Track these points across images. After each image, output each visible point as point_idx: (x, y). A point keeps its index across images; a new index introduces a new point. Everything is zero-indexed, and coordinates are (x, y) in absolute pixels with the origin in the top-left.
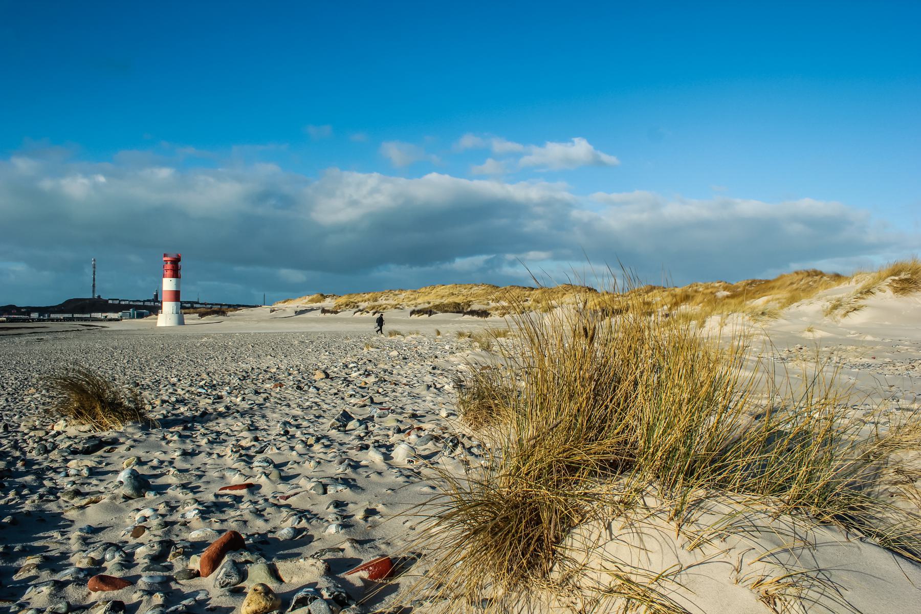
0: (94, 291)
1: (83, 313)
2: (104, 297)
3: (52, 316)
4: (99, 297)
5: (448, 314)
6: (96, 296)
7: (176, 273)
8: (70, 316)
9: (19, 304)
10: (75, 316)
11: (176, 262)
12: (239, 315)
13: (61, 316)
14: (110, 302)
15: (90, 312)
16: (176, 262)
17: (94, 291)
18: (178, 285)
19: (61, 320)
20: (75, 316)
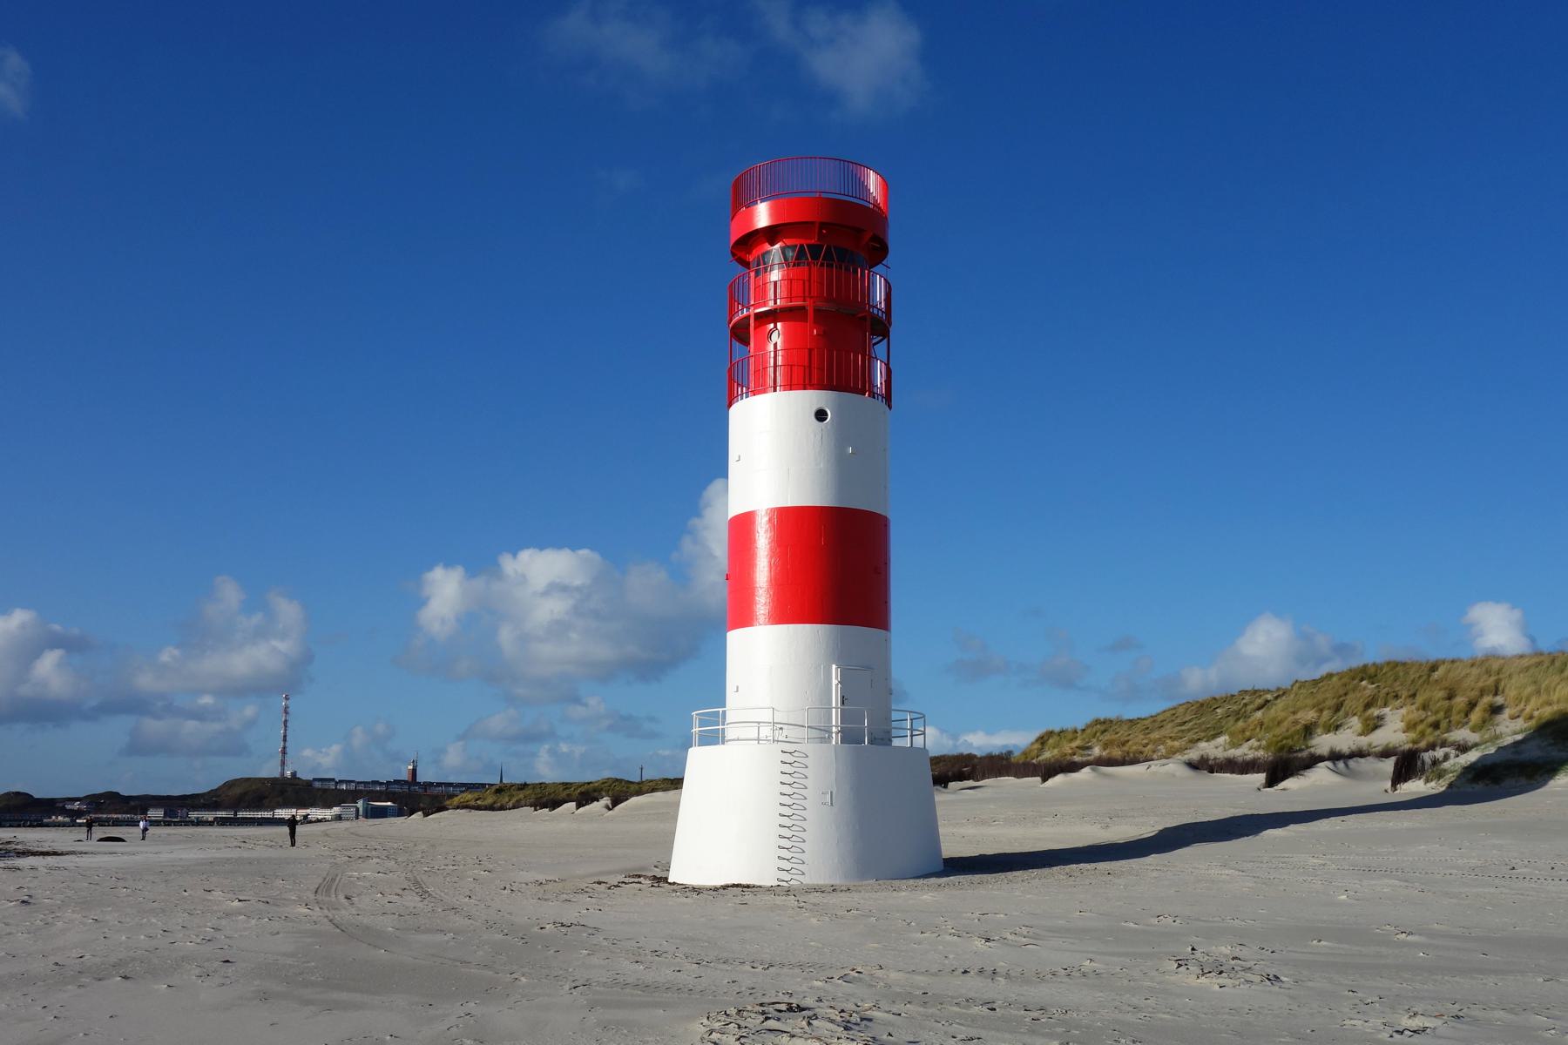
0: (283, 763)
1: (259, 808)
2: (305, 775)
3: (194, 815)
4: (294, 774)
5: (1292, 827)
6: (288, 773)
7: (840, 350)
8: (230, 814)
9: (125, 791)
10: (241, 814)
11: (842, 241)
12: (1516, 733)
13: (209, 816)
14: (317, 785)
15: (273, 809)
16: (842, 241)
17: (283, 763)
18: (849, 452)
19: (210, 824)
20: (241, 814)
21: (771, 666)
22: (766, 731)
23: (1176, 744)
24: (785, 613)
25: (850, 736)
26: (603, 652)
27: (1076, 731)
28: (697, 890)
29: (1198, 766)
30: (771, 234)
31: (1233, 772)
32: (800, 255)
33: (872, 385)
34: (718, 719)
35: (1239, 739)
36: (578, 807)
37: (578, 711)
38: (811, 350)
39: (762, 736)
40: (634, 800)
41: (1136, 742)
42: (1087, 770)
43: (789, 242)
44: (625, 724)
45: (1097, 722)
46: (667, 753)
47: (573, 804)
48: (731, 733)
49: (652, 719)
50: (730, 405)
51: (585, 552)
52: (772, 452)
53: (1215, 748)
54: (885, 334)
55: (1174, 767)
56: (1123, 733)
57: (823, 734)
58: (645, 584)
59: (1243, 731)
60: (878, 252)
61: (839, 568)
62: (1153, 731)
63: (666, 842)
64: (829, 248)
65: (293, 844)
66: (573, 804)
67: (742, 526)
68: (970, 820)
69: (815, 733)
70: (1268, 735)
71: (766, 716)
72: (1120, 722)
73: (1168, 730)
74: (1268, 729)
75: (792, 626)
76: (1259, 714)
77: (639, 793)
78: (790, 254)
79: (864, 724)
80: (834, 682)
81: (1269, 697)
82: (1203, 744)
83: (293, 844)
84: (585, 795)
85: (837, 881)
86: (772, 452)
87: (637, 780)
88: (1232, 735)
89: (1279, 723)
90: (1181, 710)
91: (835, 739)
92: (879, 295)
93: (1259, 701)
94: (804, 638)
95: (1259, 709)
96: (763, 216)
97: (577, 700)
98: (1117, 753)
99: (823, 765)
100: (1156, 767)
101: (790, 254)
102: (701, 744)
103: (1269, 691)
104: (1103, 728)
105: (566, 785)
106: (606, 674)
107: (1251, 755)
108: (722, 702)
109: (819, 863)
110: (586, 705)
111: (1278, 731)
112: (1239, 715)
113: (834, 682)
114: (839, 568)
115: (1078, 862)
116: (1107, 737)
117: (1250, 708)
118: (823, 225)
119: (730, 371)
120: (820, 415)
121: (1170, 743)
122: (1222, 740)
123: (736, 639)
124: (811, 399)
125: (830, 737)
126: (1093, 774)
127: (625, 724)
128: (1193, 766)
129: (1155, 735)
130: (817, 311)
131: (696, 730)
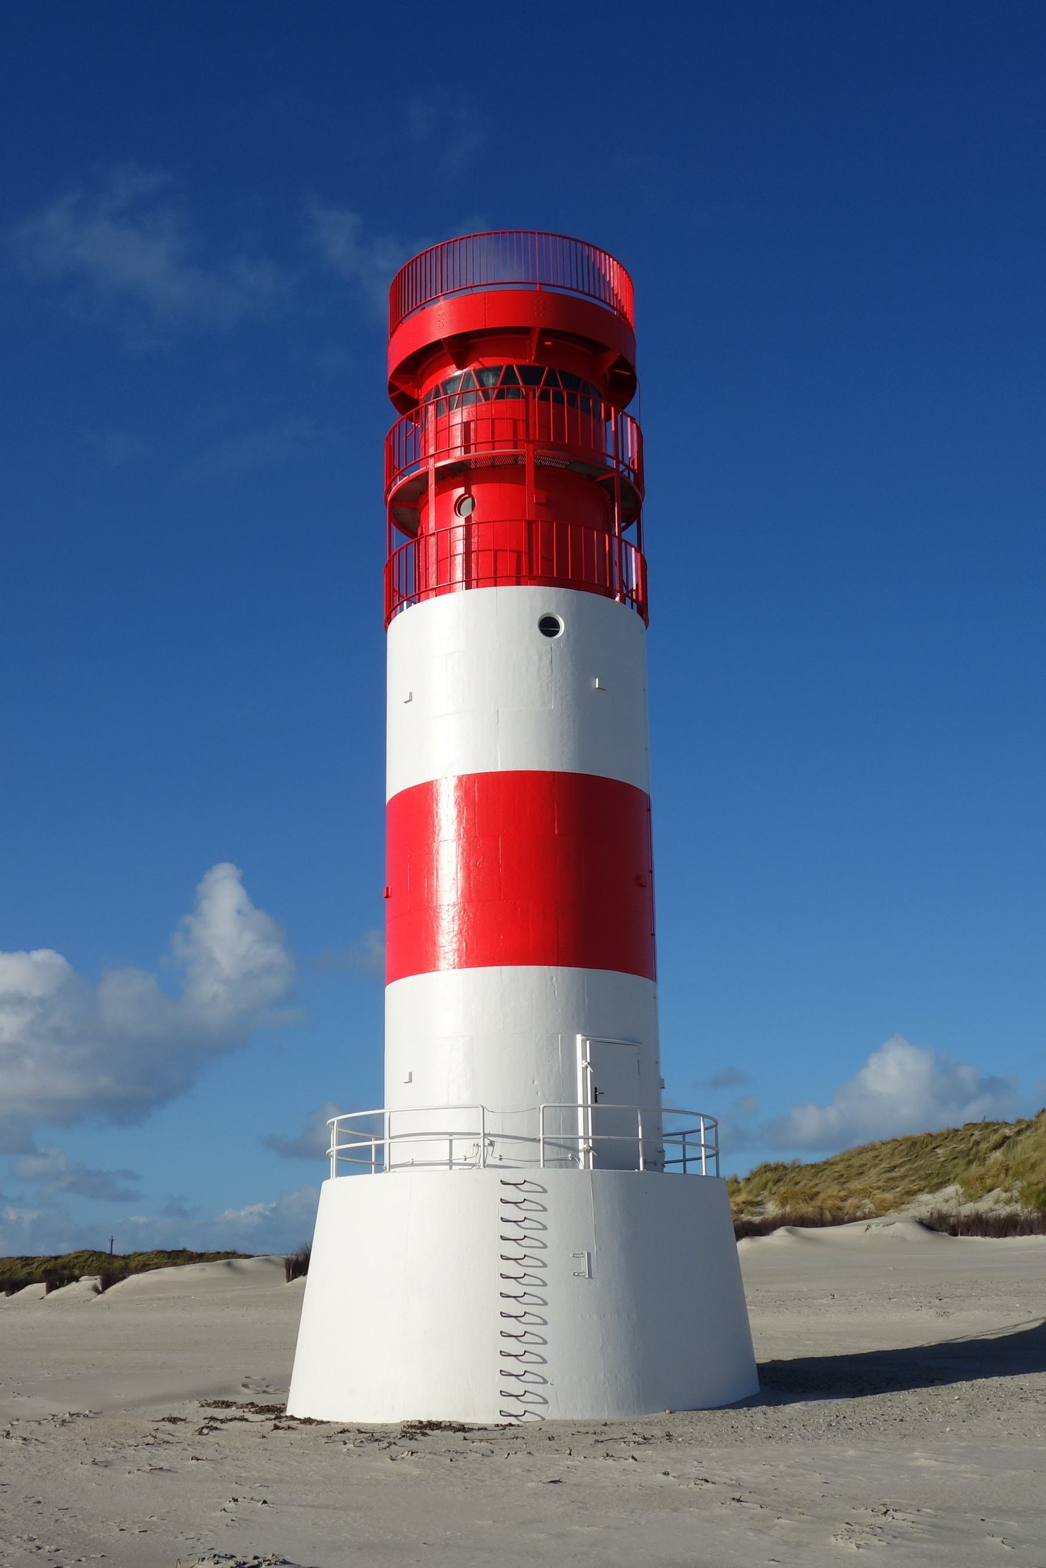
7: (568, 528)
11: (569, 362)
16: (569, 362)
18: (590, 695)
21: (462, 1035)
22: (463, 1149)
23: (889, 1196)
24: (485, 948)
25: (609, 1156)
26: (67, 1086)
27: (736, 1181)
28: (370, 1436)
29: (936, 1225)
30: (460, 348)
31: (985, 1234)
32: (509, 377)
33: (625, 584)
34: (375, 1127)
35: (976, 1189)
36: (50, 1289)
37: (33, 1164)
38: (530, 523)
39: (458, 1156)
40: (133, 1279)
41: (830, 1193)
42: (781, 1232)
43: (489, 362)
44: (93, 1184)
45: (767, 1168)
46: (142, 1220)
47: (43, 1286)
48: (396, 1152)
49: (129, 1175)
50: (389, 620)
51: (40, 956)
52: (463, 684)
53: (948, 1199)
54: (632, 515)
55: (899, 1227)
56: (805, 1183)
57: (562, 1152)
58: (124, 997)
59: (982, 1178)
60: (622, 386)
61: (574, 873)
62: (849, 1179)
63: (284, 1346)
64: (551, 372)
65: (411, 1074)
66: (43, 1286)
67: (421, 797)
68: (806, 1297)
69: (553, 1152)
70: (1019, 1184)
71: (458, 1122)
72: (798, 1168)
73: (872, 1177)
74: (1018, 1176)
75: (506, 970)
76: (998, 1154)
77: (144, 1268)
78: (490, 381)
79: (628, 1137)
80: (580, 1063)
81: (1007, 1132)
82: (925, 1197)
83: (411, 1074)
84: (57, 1274)
85: (605, 1416)
86: (463, 684)
87: (108, 1252)
88: (964, 1183)
89: (1033, 1167)
90: (886, 1150)
91: (584, 1161)
92: (630, 451)
93: (995, 1138)
94: (526, 988)
95: (997, 1147)
96: (440, 321)
97: (29, 1149)
98: (807, 1209)
99: (572, 1202)
100: (876, 1226)
101: (490, 381)
102: (339, 1174)
103: (1006, 1124)
104: (774, 1176)
105: (26, 1261)
106: (69, 1114)
107: (1004, 1211)
108: (376, 1096)
109: (571, 1386)
110: (45, 1155)
111: (1033, 1178)
112: (971, 1156)
113: (580, 1063)
114: (574, 873)
115: (987, 1376)
116: (783, 1188)
117: (983, 1146)
118: (545, 333)
119: (389, 565)
120: (548, 626)
121: (880, 1196)
122: (951, 1190)
123: (402, 996)
124: (528, 601)
125: (575, 1159)
126: (791, 1239)
127: (93, 1184)
128: (936, 1225)
129: (856, 1185)
130: (538, 468)
131: (334, 1148)
